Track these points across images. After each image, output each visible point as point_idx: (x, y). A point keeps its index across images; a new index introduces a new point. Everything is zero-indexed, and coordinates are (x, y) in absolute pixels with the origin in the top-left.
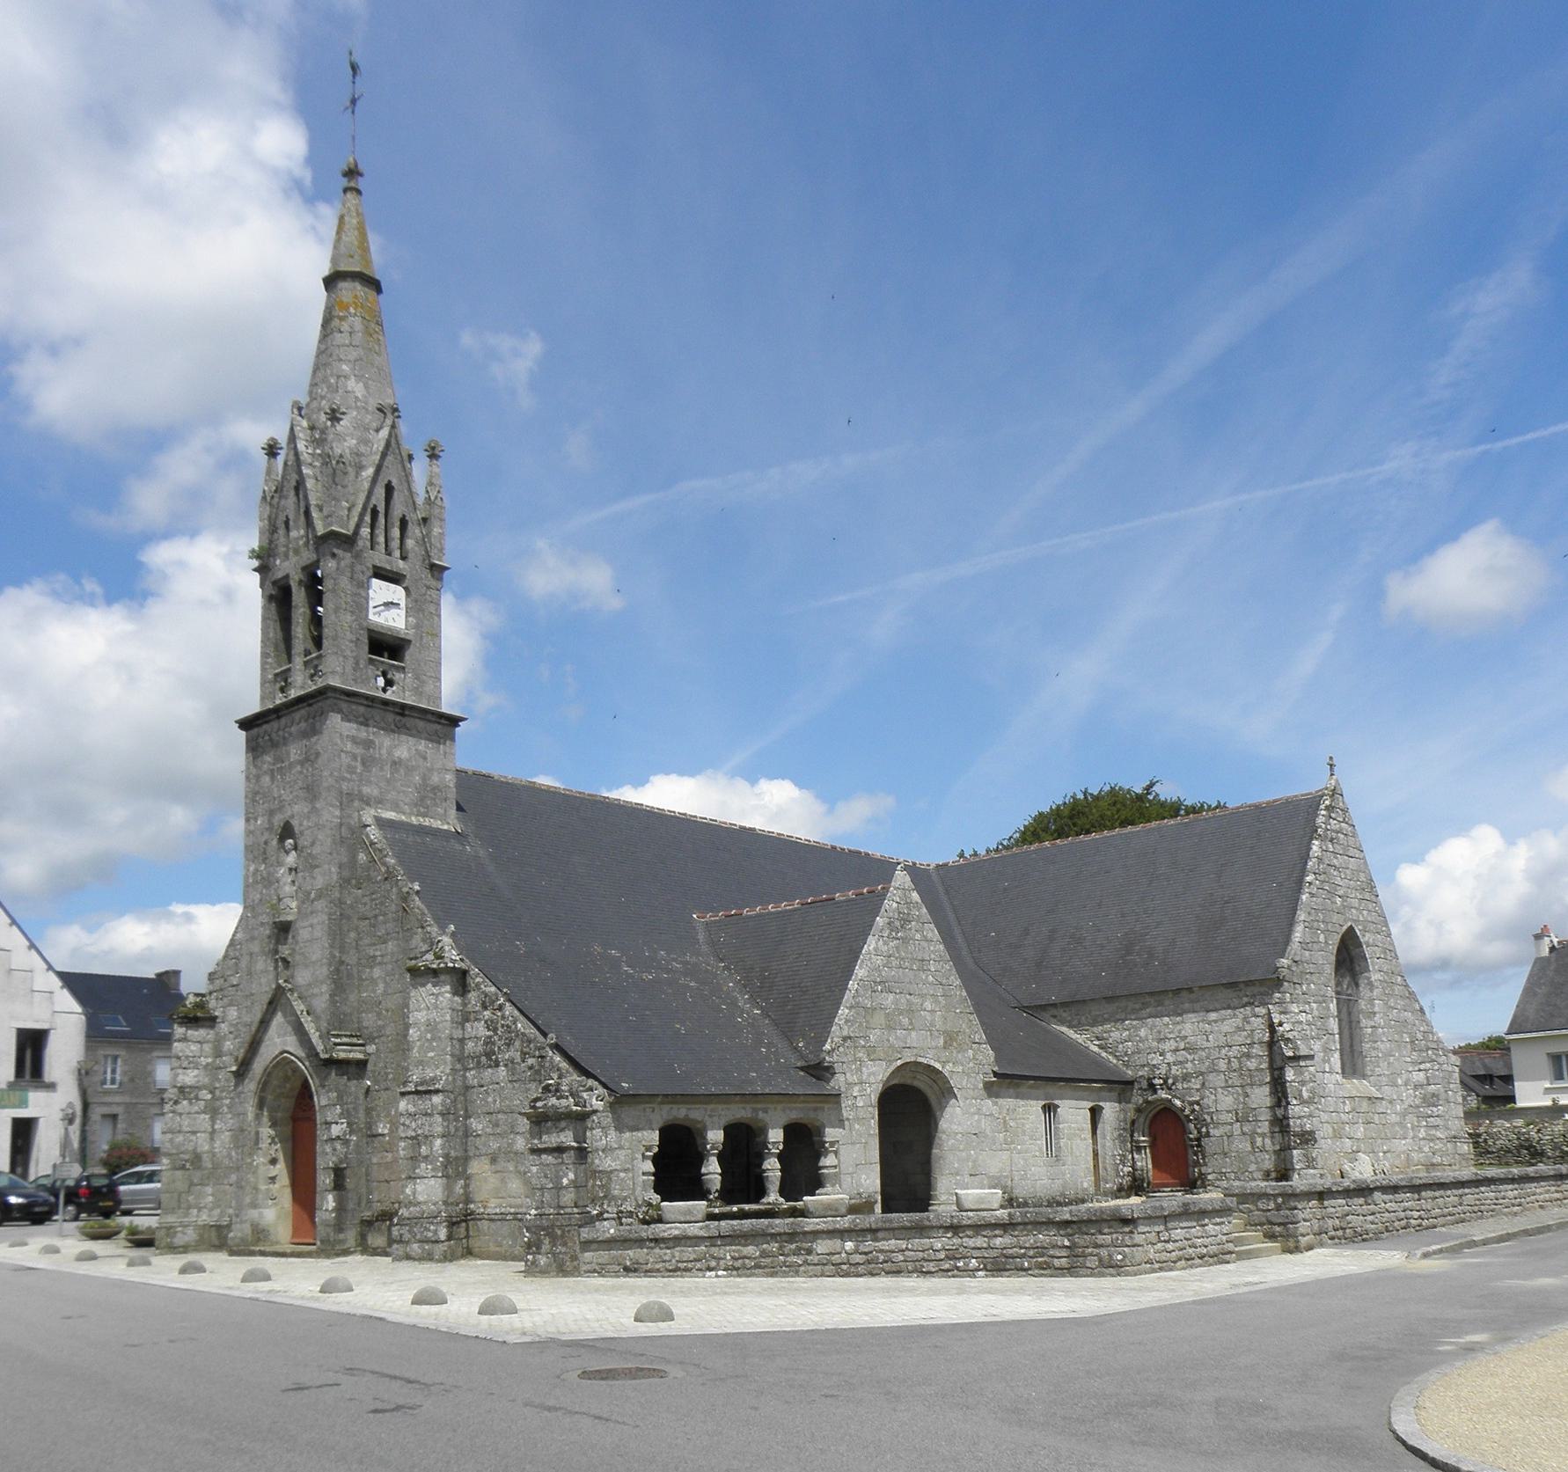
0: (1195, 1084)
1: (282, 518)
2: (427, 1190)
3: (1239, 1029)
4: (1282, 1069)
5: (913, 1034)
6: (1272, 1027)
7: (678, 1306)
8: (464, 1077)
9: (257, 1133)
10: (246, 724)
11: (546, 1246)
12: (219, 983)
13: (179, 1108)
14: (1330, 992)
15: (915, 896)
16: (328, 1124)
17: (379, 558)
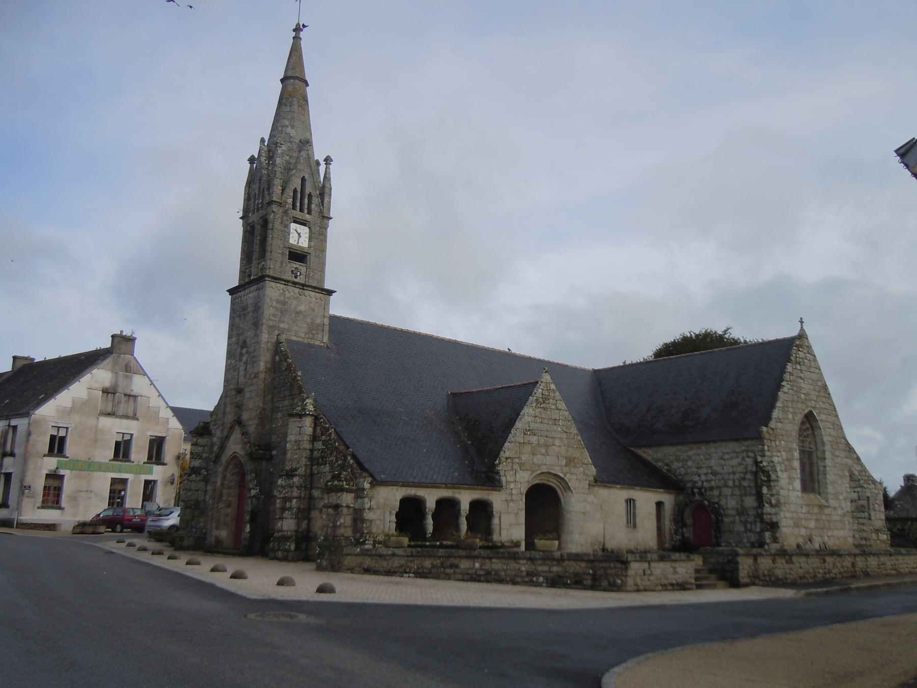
0: (716, 493)
1: (253, 193)
2: (288, 525)
3: (740, 464)
4: (761, 487)
5: (548, 458)
6: (756, 463)
7: (337, 586)
8: (311, 469)
9: (221, 493)
10: (232, 291)
11: (326, 556)
12: (214, 417)
13: (191, 478)
14: (795, 446)
15: (553, 386)
16: (250, 490)
17: (297, 213)
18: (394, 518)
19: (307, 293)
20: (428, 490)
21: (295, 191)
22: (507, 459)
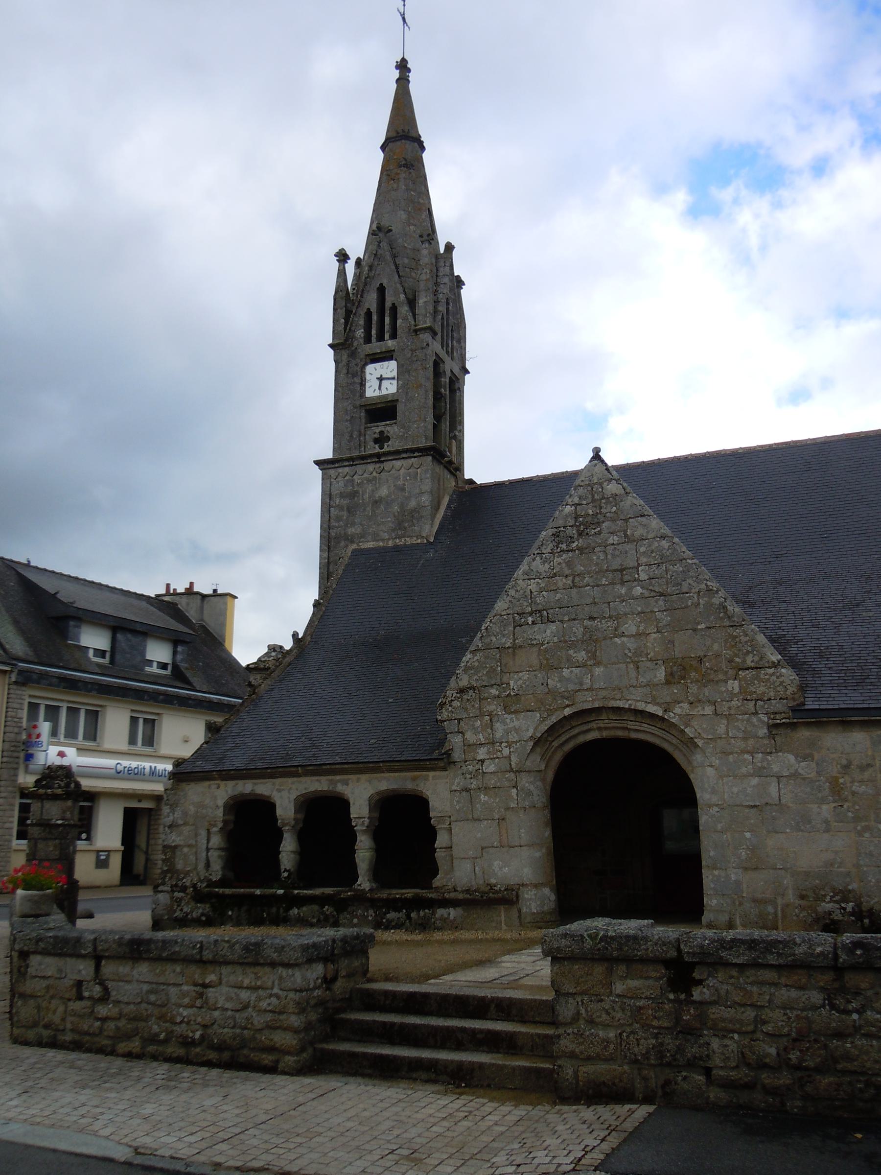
5: (598, 671)
18: (216, 840)
19: (387, 465)
20: (278, 781)
21: (369, 314)
22: (462, 691)
